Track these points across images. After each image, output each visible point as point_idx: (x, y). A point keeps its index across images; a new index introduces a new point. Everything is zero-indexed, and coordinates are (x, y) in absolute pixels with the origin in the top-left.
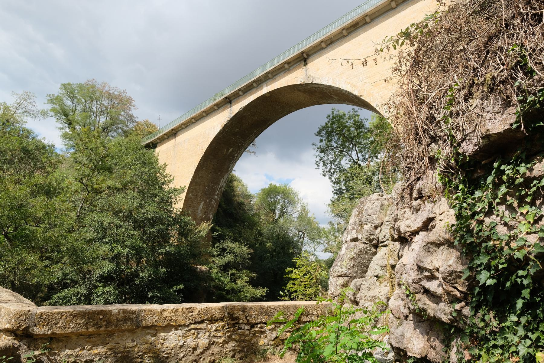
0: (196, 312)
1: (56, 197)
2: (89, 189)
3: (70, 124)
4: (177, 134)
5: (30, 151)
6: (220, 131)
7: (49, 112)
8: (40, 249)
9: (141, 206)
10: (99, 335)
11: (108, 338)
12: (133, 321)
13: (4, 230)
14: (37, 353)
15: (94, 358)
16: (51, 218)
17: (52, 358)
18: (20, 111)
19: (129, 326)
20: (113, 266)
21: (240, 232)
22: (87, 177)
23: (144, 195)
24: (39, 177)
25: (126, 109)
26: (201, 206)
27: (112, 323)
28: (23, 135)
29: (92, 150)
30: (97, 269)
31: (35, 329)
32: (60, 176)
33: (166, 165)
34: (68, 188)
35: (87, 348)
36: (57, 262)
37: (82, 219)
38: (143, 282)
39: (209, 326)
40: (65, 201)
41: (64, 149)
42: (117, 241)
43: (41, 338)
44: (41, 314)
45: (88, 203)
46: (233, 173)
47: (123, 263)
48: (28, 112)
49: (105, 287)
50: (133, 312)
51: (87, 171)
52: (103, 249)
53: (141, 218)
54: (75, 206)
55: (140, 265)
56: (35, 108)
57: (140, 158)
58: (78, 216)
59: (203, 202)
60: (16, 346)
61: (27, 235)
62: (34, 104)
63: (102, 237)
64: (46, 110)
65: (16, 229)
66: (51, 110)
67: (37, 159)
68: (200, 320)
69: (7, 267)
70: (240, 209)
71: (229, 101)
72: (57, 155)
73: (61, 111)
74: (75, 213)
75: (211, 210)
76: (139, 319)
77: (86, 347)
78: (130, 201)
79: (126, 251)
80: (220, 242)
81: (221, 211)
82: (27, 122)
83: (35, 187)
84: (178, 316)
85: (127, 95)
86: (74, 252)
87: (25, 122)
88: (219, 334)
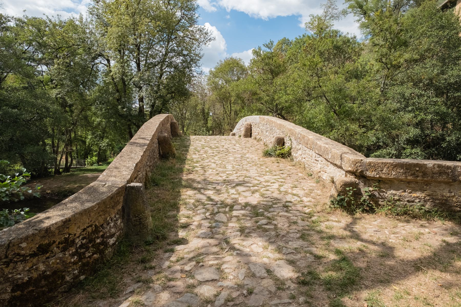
1: (363, 78)
2: (389, 66)
3: (365, 13)
5: (340, 47)
7: (348, 10)
8: (358, 120)
9: (443, 73)
10: (417, 183)
11: (425, 187)
12: (449, 175)
13: (333, 109)
14: (371, 189)
15: (414, 200)
16: (362, 95)
17: (382, 194)
18: (328, 18)
19: (445, 179)
20: (417, 131)
22: (385, 56)
23: (444, 61)
24: (349, 65)
27: (428, 175)
28: (333, 36)
29: (387, 30)
30: (404, 133)
31: (368, 173)
32: (363, 61)
34: (371, 70)
35: (407, 191)
36: (371, 129)
37: (386, 93)
38: (450, 145)
40: (370, 81)
41: (364, 38)
42: (420, 109)
43: (372, 180)
44: (370, 163)
45: (389, 78)
47: (428, 129)
48: (333, 16)
49: (412, 149)
50: (449, 168)
51: (385, 50)
52: (408, 117)
53: (444, 84)
54: (379, 83)
55: (445, 129)
56: (337, 11)
57: (437, 23)
58: (382, 91)
60: (357, 182)
61: (347, 110)
62: (336, 8)
63: (405, 106)
64: (345, 9)
65: (340, 107)
66: (349, 8)
67: (345, 52)
69: (339, 133)
72: (359, 44)
73: (356, 5)
74: (379, 89)
76: (455, 174)
77: (407, 190)
78: (429, 70)
79: (429, 117)
83: (347, 74)
86: (383, 120)
87: (332, 25)
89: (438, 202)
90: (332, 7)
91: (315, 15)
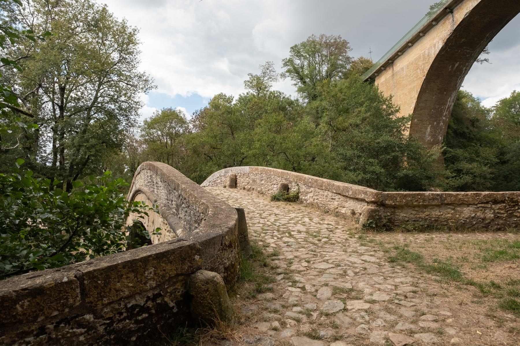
0: (482, 196)
4: (394, 63)
6: (442, 47)
18: (266, 78)
21: (476, 151)
25: (342, 53)
26: (429, 130)
31: (386, 202)
33: (391, 97)
39: (493, 206)
43: (389, 207)
46: (461, 89)
56: (274, 73)
59: (430, 126)
66: (287, 72)
68: (485, 201)
70: (474, 127)
71: (449, 10)
75: (439, 133)
80: (453, 163)
81: (450, 132)
82: (272, 86)
84: (469, 198)
85: (341, 40)
88: (502, 212)
89: (433, 219)
90: (270, 69)
91: (254, 75)
